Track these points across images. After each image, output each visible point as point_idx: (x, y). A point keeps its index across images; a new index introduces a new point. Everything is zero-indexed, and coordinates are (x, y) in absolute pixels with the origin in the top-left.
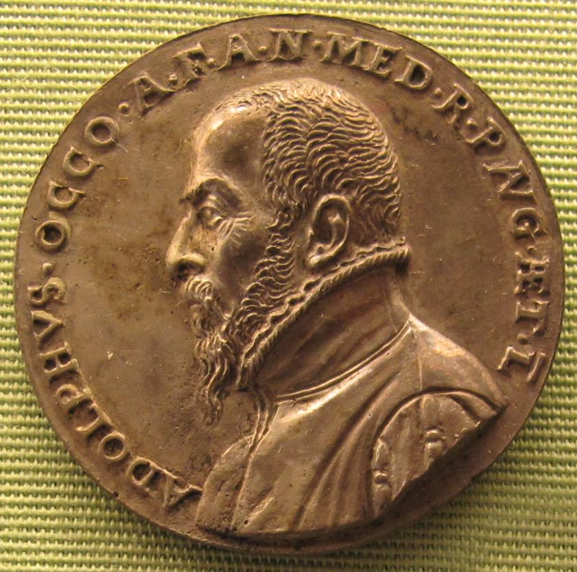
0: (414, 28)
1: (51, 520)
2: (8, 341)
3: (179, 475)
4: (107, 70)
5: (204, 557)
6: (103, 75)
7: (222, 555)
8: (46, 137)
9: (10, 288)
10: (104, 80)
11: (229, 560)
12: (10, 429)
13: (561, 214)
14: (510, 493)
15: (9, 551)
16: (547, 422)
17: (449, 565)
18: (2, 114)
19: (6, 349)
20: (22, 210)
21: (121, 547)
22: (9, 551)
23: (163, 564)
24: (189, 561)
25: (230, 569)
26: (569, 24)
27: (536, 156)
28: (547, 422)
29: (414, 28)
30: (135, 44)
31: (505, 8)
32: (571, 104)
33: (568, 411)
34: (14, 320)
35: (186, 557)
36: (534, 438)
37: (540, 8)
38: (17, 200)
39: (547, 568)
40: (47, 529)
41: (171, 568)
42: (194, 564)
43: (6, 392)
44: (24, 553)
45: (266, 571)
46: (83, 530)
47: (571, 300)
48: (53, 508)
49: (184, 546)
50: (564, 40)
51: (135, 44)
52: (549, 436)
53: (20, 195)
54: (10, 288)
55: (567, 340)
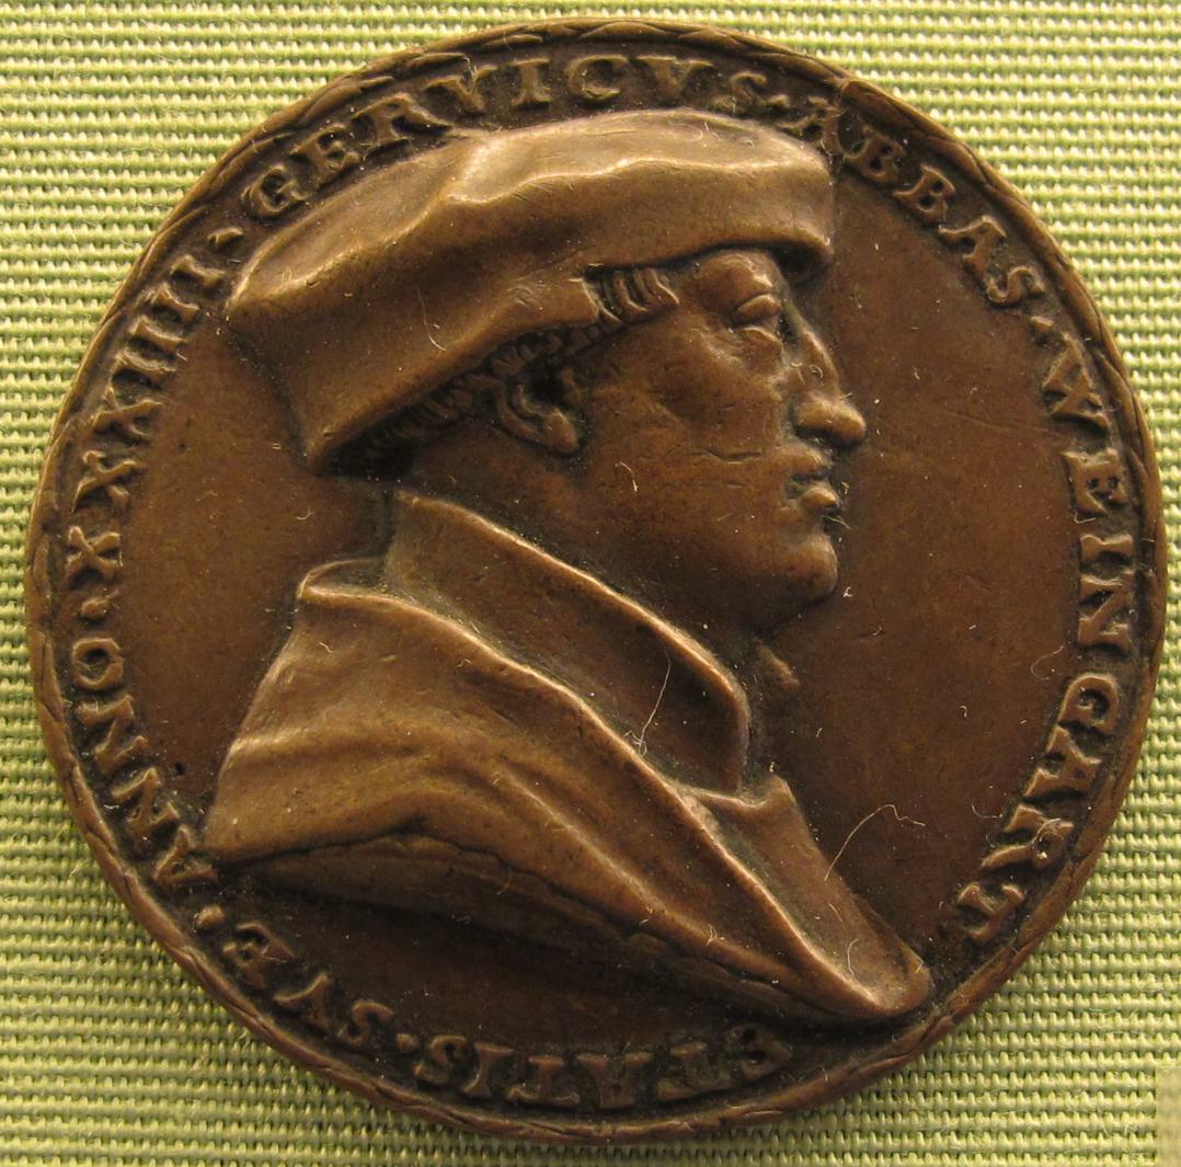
1: (68, 901)
2: (14, 667)
6: (221, 141)
7: (406, 1120)
9: (20, 573)
13: (1107, 303)
15: (16, 1115)
16: (1043, 965)
17: (1039, 965)
18: (4, 267)
19: (11, 680)
21: (127, 1005)
22: (16, 1115)
26: (1169, 266)
27: (1122, 354)
28: (1075, 1003)
30: (206, 141)
31: (919, 15)
32: (1170, 371)
34: (30, 689)
40: (37, 1037)
43: (11, 894)
44: (98, 263)
46: (87, 997)
47: (1174, 509)
50: (107, 1095)
51: (206, 141)
53: (24, 488)
54: (20, 573)
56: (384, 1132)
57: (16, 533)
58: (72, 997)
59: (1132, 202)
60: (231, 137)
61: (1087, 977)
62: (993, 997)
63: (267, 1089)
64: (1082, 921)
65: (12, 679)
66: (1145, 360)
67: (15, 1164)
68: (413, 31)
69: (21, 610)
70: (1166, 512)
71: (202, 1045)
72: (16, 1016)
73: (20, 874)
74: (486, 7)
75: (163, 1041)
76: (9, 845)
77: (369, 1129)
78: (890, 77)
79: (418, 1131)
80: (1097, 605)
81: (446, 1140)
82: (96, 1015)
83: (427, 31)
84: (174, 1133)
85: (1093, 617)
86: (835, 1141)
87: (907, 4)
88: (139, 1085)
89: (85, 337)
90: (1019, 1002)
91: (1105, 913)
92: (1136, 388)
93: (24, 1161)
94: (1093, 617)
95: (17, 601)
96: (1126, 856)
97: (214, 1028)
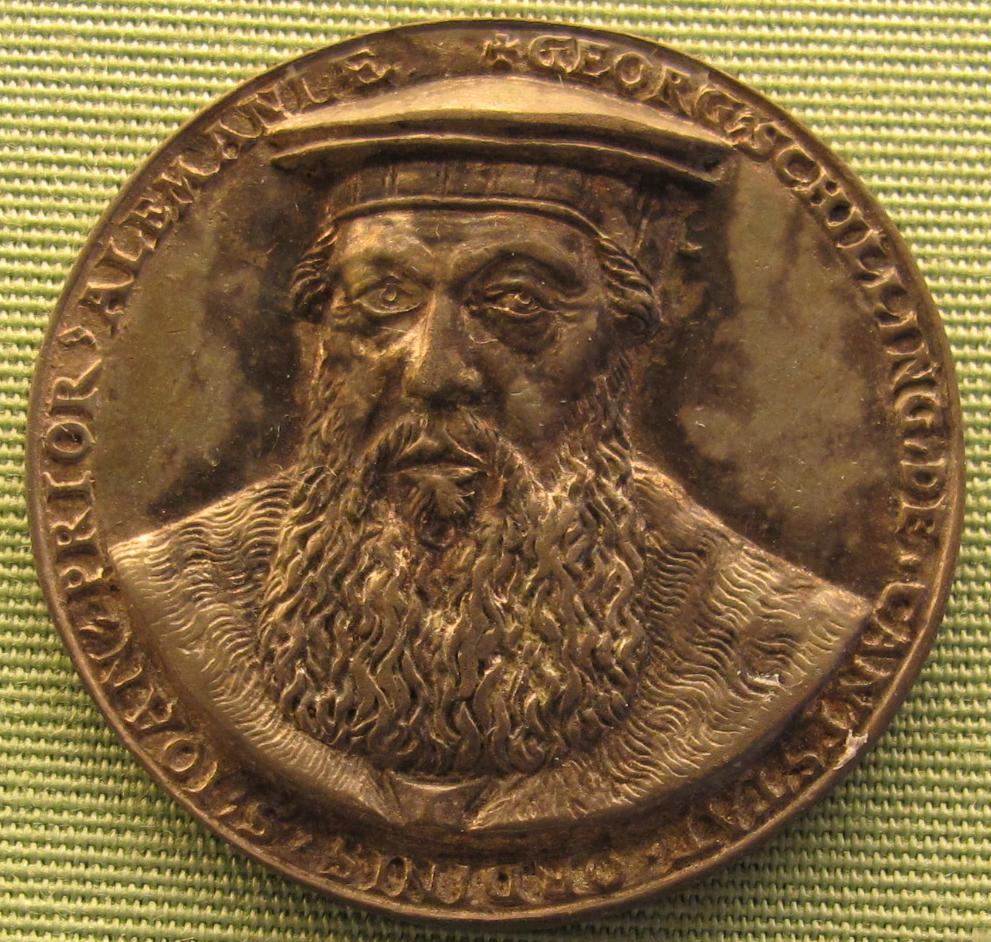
0: (703, 45)
3: (464, 771)
4: (166, 121)
5: (321, 912)
6: (162, 128)
7: (320, 907)
8: (101, 190)
10: (165, 137)
11: (344, 916)
12: (138, 890)
14: (836, 849)
20: (54, 302)
23: (271, 892)
24: (267, 915)
25: (433, 937)
29: (809, 113)
33: (917, 756)
35: (321, 913)
36: (901, 785)
37: (886, 13)
38: (59, 269)
39: (813, 935)
41: (323, 934)
42: (333, 927)
45: (476, 941)
48: (53, 864)
49: (254, 875)
52: (893, 780)
53: (55, 279)
55: (949, 646)
56: (230, 878)
57: (14, 434)
58: (159, 902)
59: (956, 95)
60: (171, 126)
61: (958, 807)
62: (855, 770)
63: (197, 876)
64: (896, 755)
65: (10, 444)
66: (967, 350)
67: (55, 939)
68: (344, 24)
69: (24, 403)
70: (960, 386)
71: (299, 934)
72: (13, 96)
73: (17, 752)
74: (128, 6)
75: (230, 910)
76: (8, 553)
77: (287, 914)
78: (735, 63)
79: (316, 915)
80: (533, 595)
81: (355, 927)
82: (160, 900)
83: (359, 25)
84: (64, 768)
85: (357, 656)
86: (862, 790)
87: (243, 4)
88: (22, 726)
89: (67, 262)
90: (852, 824)
91: (901, 785)
92: (969, 443)
93: (48, 936)
94: (357, 656)
95: (18, 460)
96: (914, 752)
97: (150, 821)
